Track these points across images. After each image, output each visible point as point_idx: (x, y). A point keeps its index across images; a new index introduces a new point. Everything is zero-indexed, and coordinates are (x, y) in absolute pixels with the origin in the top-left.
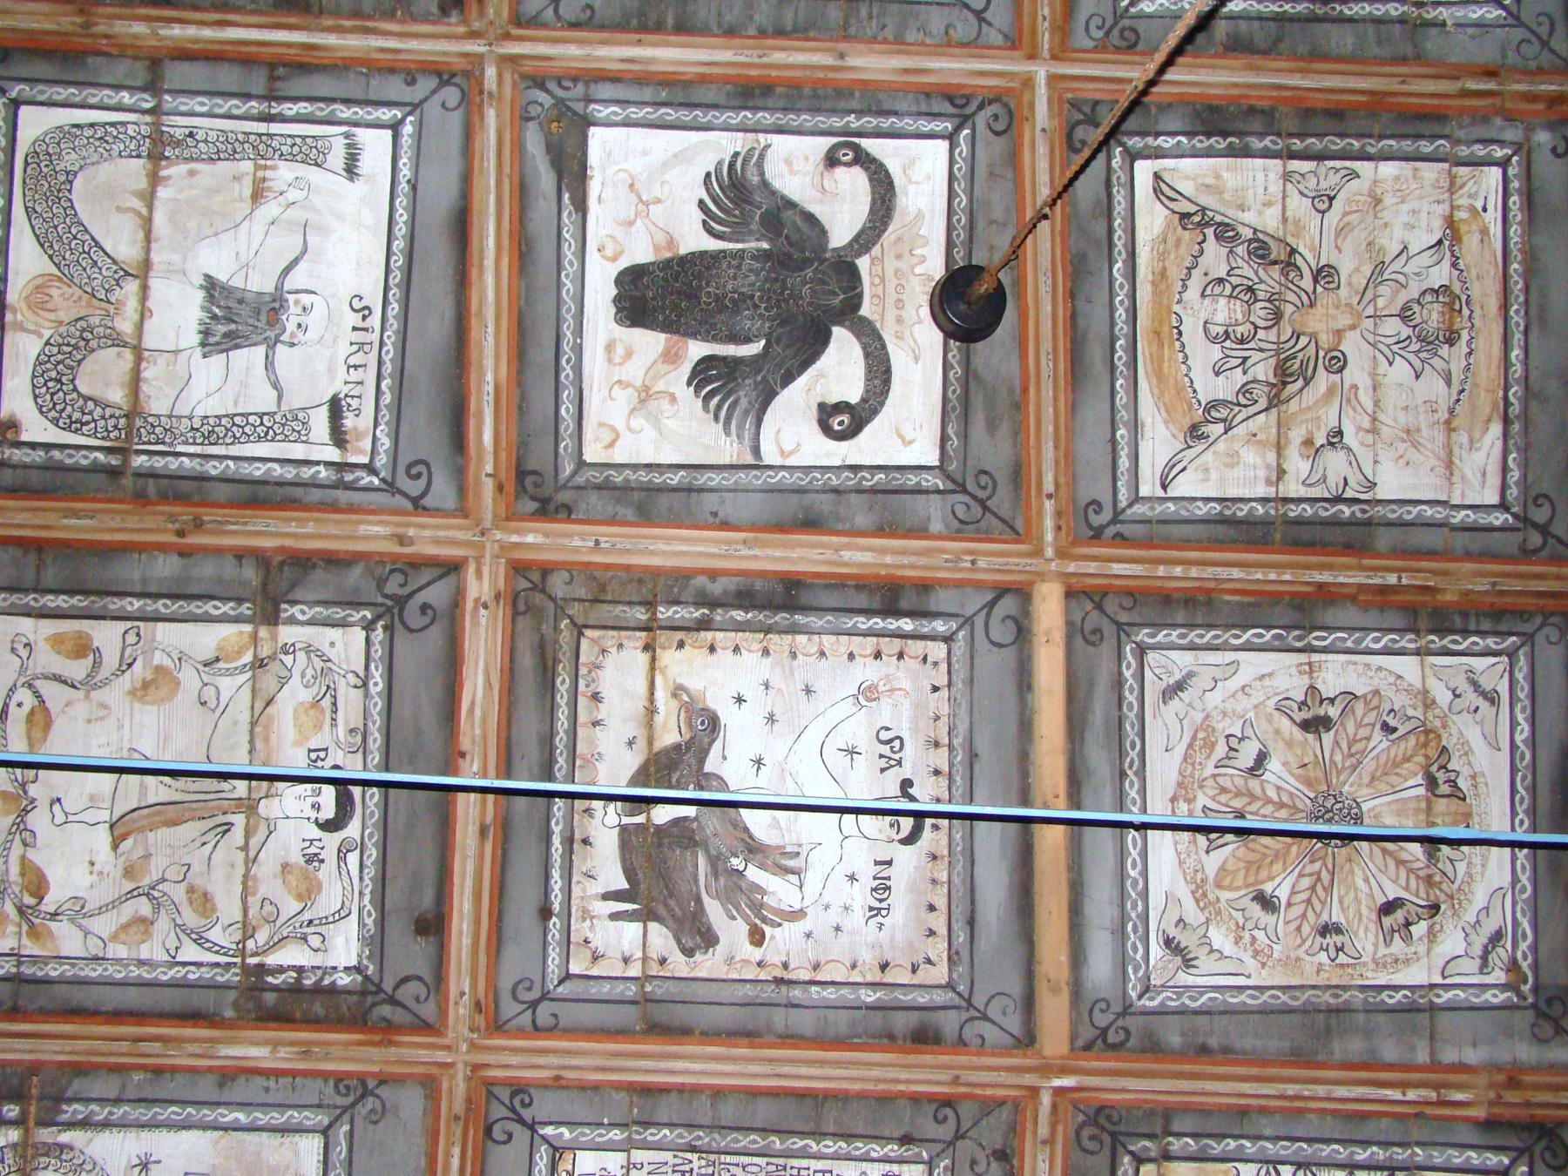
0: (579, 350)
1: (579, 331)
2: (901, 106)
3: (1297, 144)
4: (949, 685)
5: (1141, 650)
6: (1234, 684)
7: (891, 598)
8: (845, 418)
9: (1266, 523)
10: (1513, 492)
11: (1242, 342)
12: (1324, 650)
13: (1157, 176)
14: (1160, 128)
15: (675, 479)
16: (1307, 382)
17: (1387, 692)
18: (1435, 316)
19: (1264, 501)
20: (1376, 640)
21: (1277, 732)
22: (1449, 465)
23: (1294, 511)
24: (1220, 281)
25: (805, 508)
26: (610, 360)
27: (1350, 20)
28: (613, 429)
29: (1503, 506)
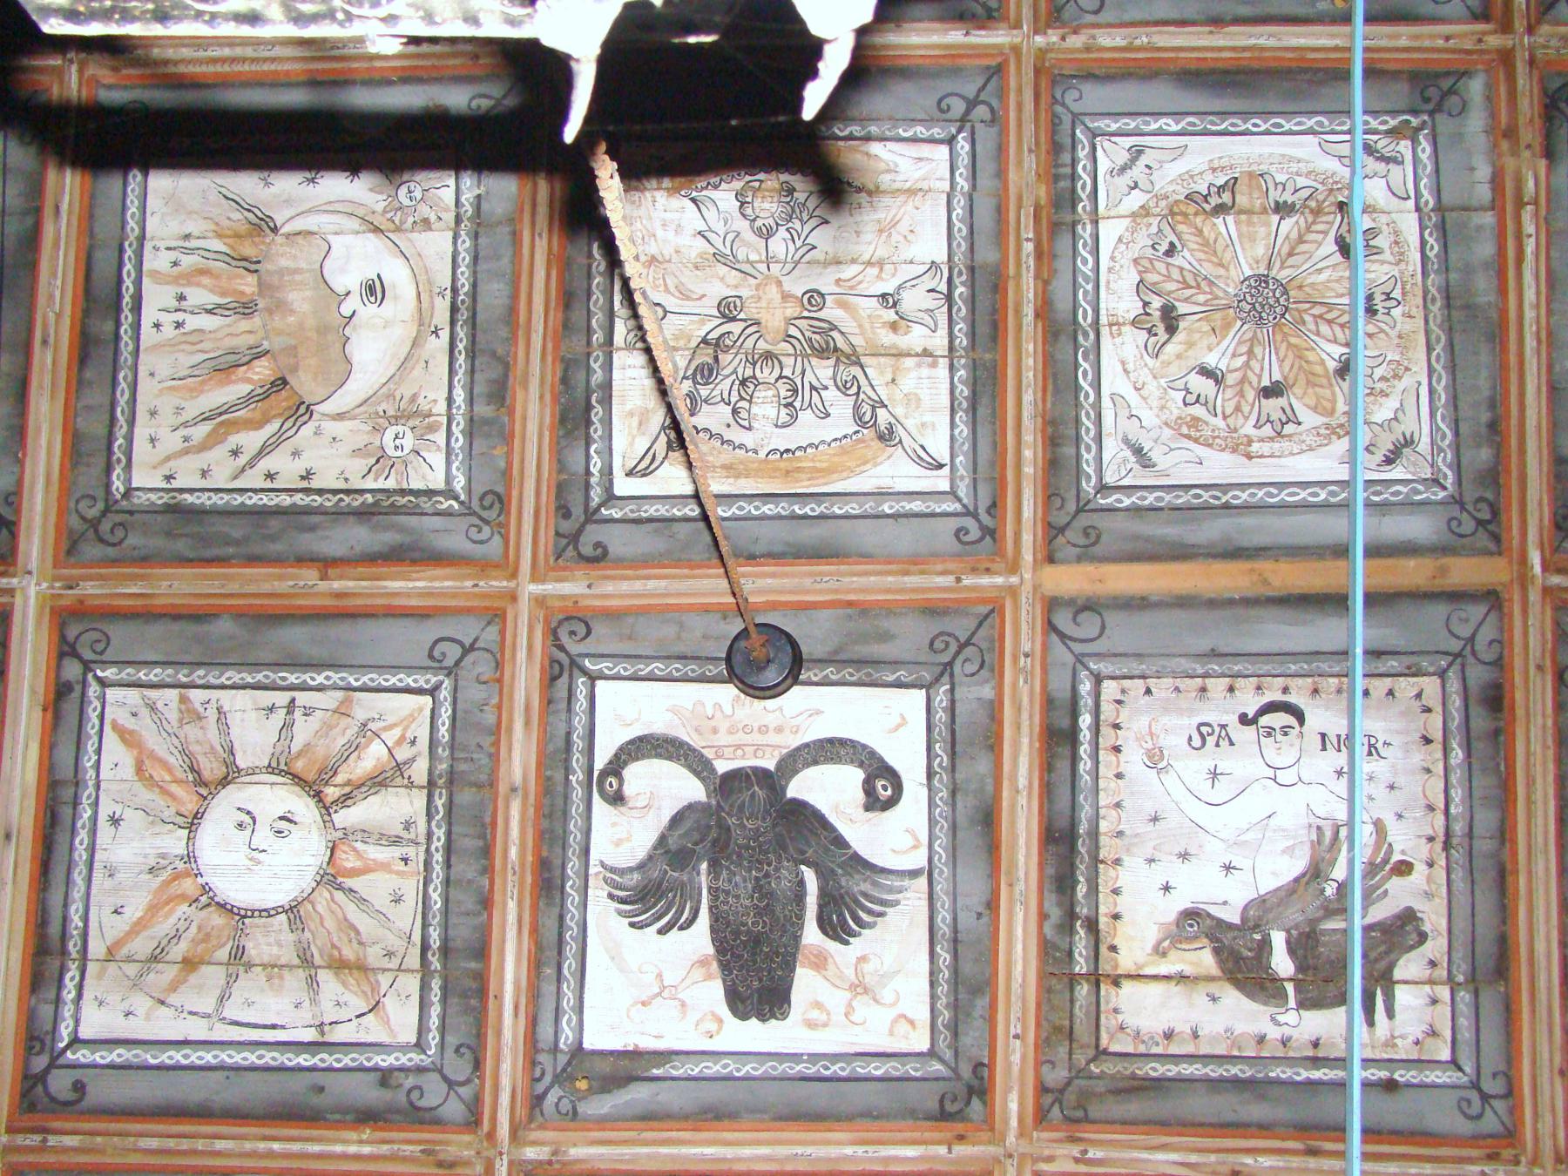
0: (814, 1058)
1: (795, 1057)
2: (562, 729)
3: (598, 337)
4: (1144, 677)
5: (1103, 488)
6: (1133, 398)
7: (1059, 738)
8: (879, 784)
9: (974, 366)
10: (936, 132)
11: (795, 391)
12: (1097, 312)
13: (630, 474)
14: (581, 470)
15: (945, 956)
16: (835, 328)
17: (1135, 251)
18: (766, 205)
19: (952, 367)
20: (1085, 262)
21: (1179, 356)
22: (911, 192)
23: (962, 340)
24: (735, 412)
25: (974, 825)
26: (825, 1025)
27: (474, 286)
28: (895, 1021)
29: (950, 141)
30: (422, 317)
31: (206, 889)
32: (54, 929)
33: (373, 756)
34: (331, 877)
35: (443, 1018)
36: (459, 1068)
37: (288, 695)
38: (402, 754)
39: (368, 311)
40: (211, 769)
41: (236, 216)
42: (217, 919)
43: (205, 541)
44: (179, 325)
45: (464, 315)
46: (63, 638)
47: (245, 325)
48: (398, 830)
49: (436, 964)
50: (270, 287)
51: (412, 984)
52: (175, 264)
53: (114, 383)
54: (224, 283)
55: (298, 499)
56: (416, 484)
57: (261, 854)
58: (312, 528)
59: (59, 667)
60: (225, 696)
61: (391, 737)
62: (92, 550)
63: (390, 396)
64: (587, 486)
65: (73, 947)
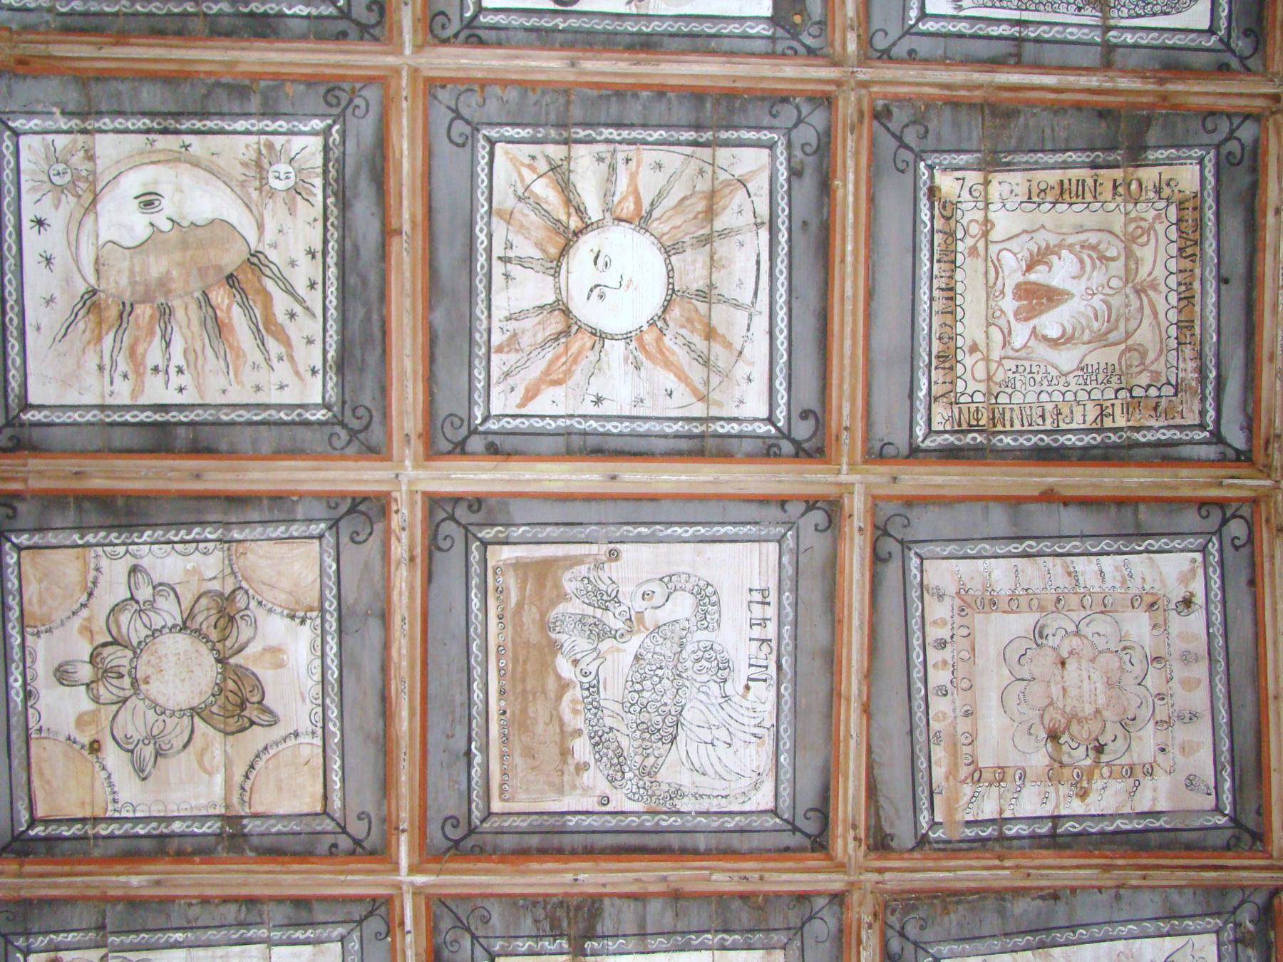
14: (306, 23)
27: (144, 114)
30: (173, 159)
31: (652, 323)
32: (684, 445)
33: (545, 190)
34: (641, 221)
35: (749, 128)
36: (787, 114)
37: (495, 262)
38: (543, 166)
39: (168, 207)
40: (556, 323)
41: (81, 325)
42: (676, 312)
43: (367, 340)
44: (180, 371)
45: (171, 124)
46: (449, 453)
47: (180, 313)
48: (604, 167)
49: (708, 135)
50: (147, 292)
51: (723, 154)
52: (125, 376)
53: (233, 424)
54: (142, 334)
55: (331, 260)
56: (319, 161)
57: (623, 277)
58: (356, 248)
59: (473, 454)
60: (498, 314)
61: (529, 176)
62: (376, 434)
63: (243, 185)
64: (320, 17)
65: (698, 429)
